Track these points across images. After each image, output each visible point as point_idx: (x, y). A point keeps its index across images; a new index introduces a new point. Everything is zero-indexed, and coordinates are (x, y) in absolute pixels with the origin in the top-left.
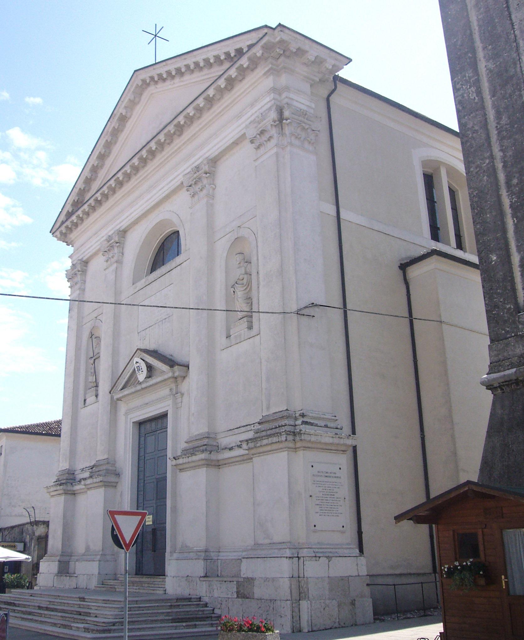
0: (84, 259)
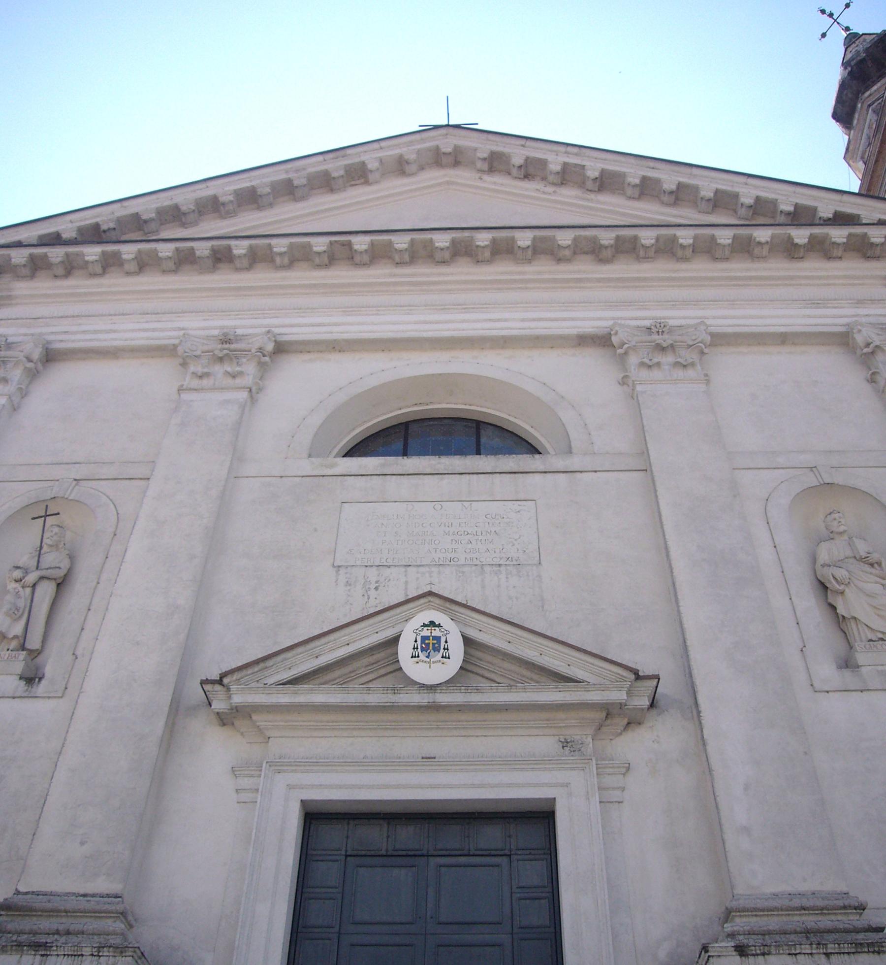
0: (10, 340)
